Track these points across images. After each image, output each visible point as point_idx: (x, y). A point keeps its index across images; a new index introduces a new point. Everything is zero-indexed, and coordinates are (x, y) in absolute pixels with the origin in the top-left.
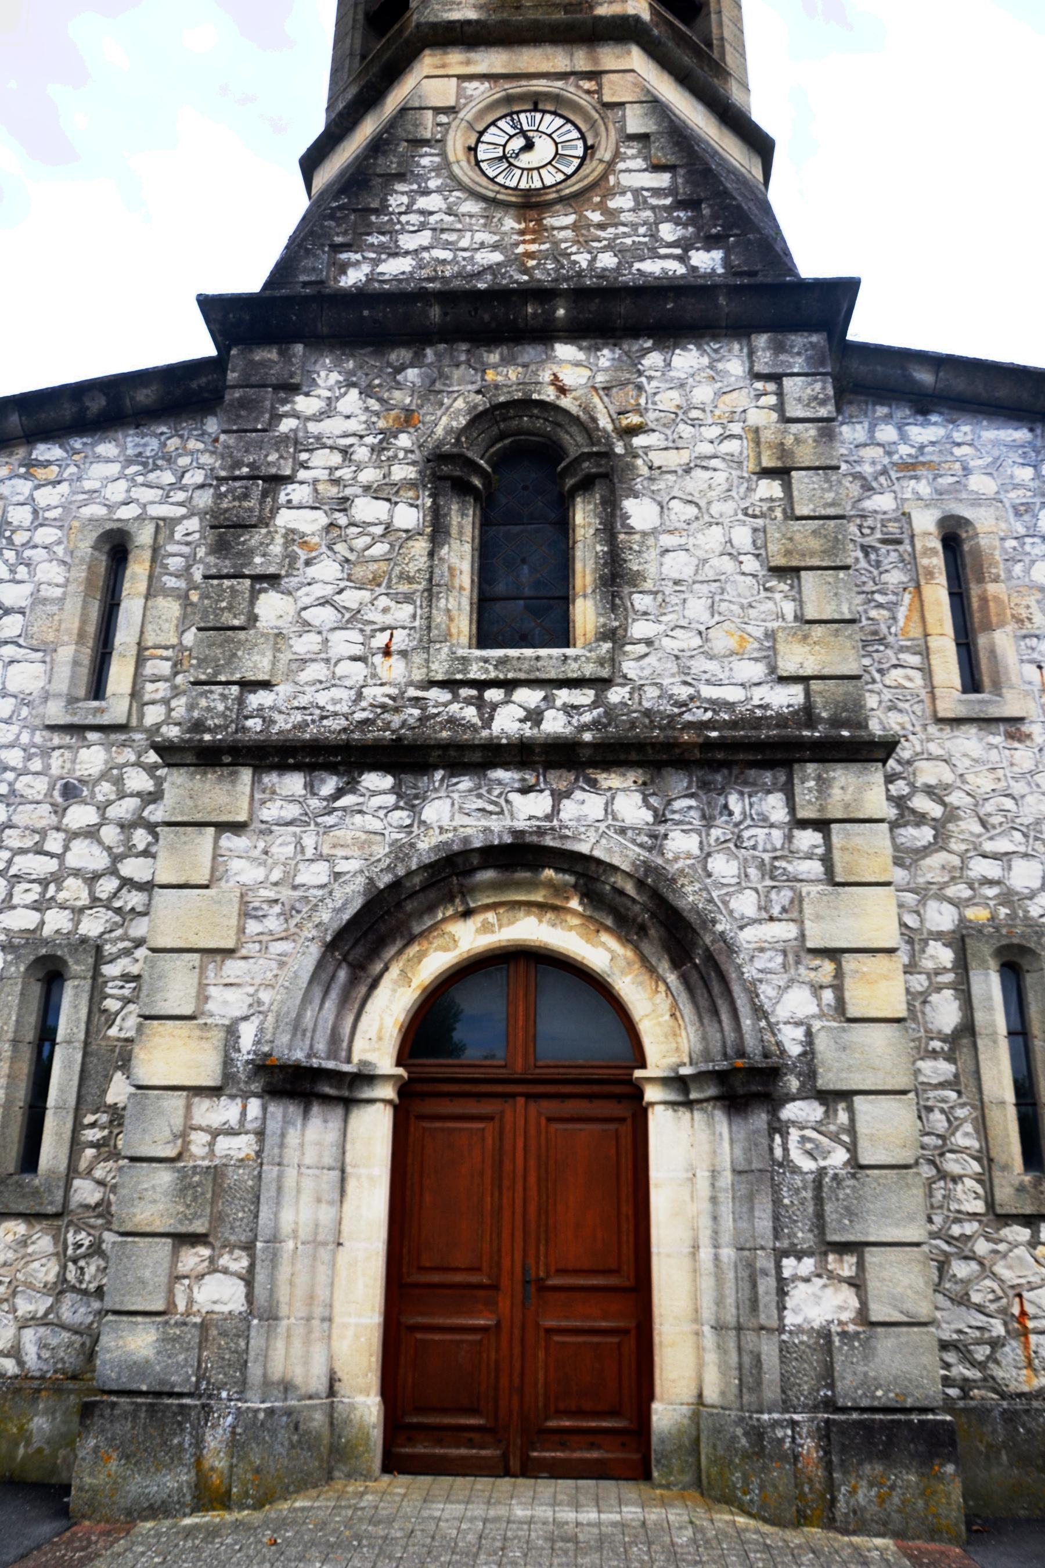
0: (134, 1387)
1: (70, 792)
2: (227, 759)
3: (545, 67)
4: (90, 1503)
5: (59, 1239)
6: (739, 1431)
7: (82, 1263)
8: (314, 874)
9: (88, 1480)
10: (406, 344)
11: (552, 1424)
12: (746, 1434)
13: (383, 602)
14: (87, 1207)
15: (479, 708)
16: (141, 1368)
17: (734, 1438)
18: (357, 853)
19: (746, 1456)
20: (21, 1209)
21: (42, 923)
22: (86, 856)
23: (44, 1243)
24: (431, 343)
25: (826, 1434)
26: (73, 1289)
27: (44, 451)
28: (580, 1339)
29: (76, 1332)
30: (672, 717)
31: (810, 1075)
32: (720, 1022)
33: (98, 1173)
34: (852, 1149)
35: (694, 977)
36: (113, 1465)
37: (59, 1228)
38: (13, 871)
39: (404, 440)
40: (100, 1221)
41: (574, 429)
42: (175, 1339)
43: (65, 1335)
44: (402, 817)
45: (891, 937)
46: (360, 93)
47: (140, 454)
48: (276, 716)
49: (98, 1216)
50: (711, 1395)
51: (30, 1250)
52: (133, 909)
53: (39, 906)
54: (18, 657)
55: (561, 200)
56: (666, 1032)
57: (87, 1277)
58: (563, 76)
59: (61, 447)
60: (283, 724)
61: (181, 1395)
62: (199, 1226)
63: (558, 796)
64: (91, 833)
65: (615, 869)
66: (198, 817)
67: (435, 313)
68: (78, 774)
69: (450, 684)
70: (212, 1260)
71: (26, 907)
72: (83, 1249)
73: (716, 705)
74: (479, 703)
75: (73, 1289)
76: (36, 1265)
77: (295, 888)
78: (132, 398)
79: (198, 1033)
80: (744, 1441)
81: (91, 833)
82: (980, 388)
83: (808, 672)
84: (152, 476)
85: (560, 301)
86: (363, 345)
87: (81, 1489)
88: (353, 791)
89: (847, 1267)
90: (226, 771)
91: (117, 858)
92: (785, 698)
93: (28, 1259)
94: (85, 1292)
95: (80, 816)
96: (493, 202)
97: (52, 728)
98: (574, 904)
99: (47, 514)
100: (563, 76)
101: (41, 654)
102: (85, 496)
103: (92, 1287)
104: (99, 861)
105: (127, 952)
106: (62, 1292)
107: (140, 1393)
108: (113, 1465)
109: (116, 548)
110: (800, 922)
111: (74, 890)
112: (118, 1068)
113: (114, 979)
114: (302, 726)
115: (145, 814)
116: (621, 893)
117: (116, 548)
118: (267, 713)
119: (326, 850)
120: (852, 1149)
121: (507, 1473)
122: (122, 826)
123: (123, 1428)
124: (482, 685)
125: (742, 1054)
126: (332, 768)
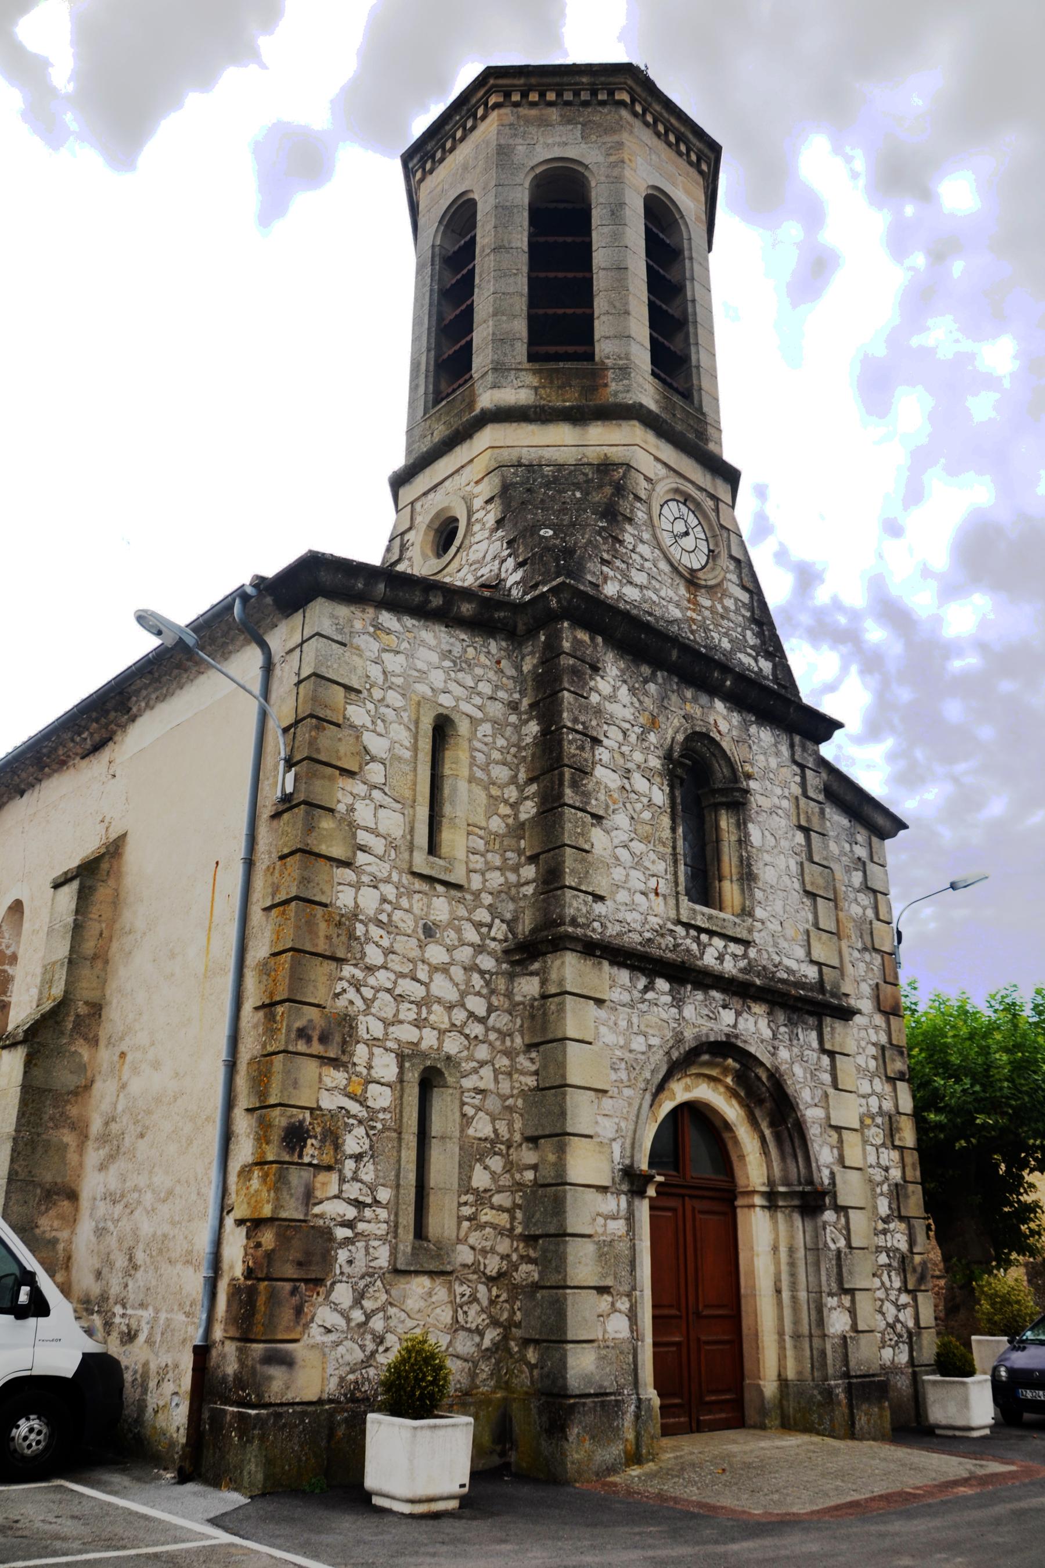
0: (587, 1391)
1: (429, 931)
2: (598, 953)
3: (693, 477)
4: (578, 1472)
5: (451, 1290)
6: (816, 1392)
7: (465, 1308)
8: (638, 1044)
9: (576, 1456)
10: (650, 663)
11: (708, 1399)
12: (820, 1393)
13: (652, 856)
14: (465, 1266)
15: (699, 945)
16: (588, 1379)
17: (813, 1396)
18: (657, 1033)
19: (820, 1405)
20: (432, 1268)
21: (421, 1038)
22: (442, 987)
23: (441, 1293)
24: (661, 670)
25: (849, 1389)
26: (463, 1328)
27: (387, 619)
28: (715, 1347)
29: (466, 1360)
30: (774, 973)
31: (835, 1196)
32: (797, 1162)
33: (471, 1241)
34: (848, 1239)
35: (785, 1134)
36: (587, 1444)
37: (450, 1282)
38: (398, 991)
39: (652, 738)
40: (475, 1277)
41: (722, 762)
42: (604, 1357)
43: (459, 1362)
44: (674, 1010)
45: (857, 1126)
46: (571, 408)
47: (450, 651)
48: (609, 925)
49: (474, 1273)
50: (791, 1374)
51: (434, 1299)
52: (476, 1037)
53: (419, 1024)
54: (384, 803)
55: (706, 587)
56: (755, 1165)
57: (470, 1319)
58: (701, 489)
59: (399, 620)
60: (613, 930)
61: (610, 1394)
62: (609, 1282)
63: (738, 1014)
64: (444, 969)
65: (762, 1064)
66: (585, 992)
67: (675, 654)
68: (432, 918)
69: (687, 926)
70: (613, 1304)
71: (409, 1023)
72: (465, 1298)
73: (789, 971)
74: (697, 940)
75: (463, 1328)
76: (438, 1310)
77: (631, 1051)
78: (459, 607)
79: (598, 1148)
80: (819, 1397)
81: (444, 969)
82: (849, 797)
83: (822, 960)
84: (460, 675)
85: (730, 677)
86: (629, 653)
87: (573, 1463)
88: (653, 989)
89: (846, 1300)
90: (596, 960)
91: (463, 994)
92: (811, 973)
93: (434, 1306)
94: (469, 1330)
95: (436, 954)
96: (675, 569)
97: (414, 874)
98: (729, 1080)
99: (394, 679)
100: (701, 489)
101: (400, 806)
102: (416, 674)
103: (473, 1326)
104: (451, 995)
105: (475, 1071)
106: (456, 1331)
107: (589, 1395)
108: (587, 1444)
109: (442, 730)
110: (827, 1109)
111: (438, 1015)
112: (478, 1160)
113: (469, 1090)
114: (620, 935)
115: (478, 961)
116: (759, 1078)
117: (442, 730)
118: (602, 919)
119: (643, 1028)
120: (848, 1239)
121: (692, 1432)
122: (465, 969)
123: (589, 1419)
124: (700, 930)
125: (810, 1182)
126: (643, 971)
